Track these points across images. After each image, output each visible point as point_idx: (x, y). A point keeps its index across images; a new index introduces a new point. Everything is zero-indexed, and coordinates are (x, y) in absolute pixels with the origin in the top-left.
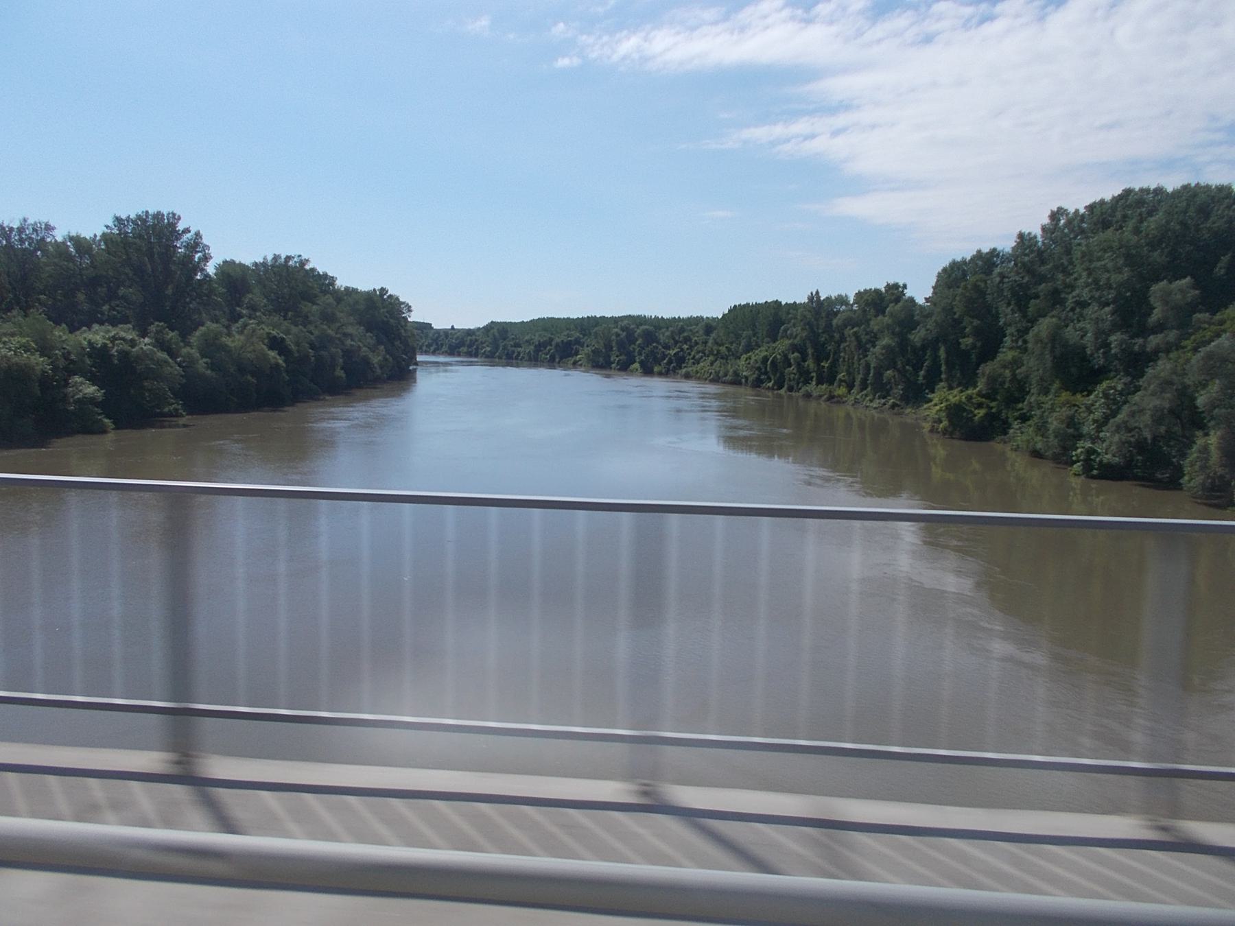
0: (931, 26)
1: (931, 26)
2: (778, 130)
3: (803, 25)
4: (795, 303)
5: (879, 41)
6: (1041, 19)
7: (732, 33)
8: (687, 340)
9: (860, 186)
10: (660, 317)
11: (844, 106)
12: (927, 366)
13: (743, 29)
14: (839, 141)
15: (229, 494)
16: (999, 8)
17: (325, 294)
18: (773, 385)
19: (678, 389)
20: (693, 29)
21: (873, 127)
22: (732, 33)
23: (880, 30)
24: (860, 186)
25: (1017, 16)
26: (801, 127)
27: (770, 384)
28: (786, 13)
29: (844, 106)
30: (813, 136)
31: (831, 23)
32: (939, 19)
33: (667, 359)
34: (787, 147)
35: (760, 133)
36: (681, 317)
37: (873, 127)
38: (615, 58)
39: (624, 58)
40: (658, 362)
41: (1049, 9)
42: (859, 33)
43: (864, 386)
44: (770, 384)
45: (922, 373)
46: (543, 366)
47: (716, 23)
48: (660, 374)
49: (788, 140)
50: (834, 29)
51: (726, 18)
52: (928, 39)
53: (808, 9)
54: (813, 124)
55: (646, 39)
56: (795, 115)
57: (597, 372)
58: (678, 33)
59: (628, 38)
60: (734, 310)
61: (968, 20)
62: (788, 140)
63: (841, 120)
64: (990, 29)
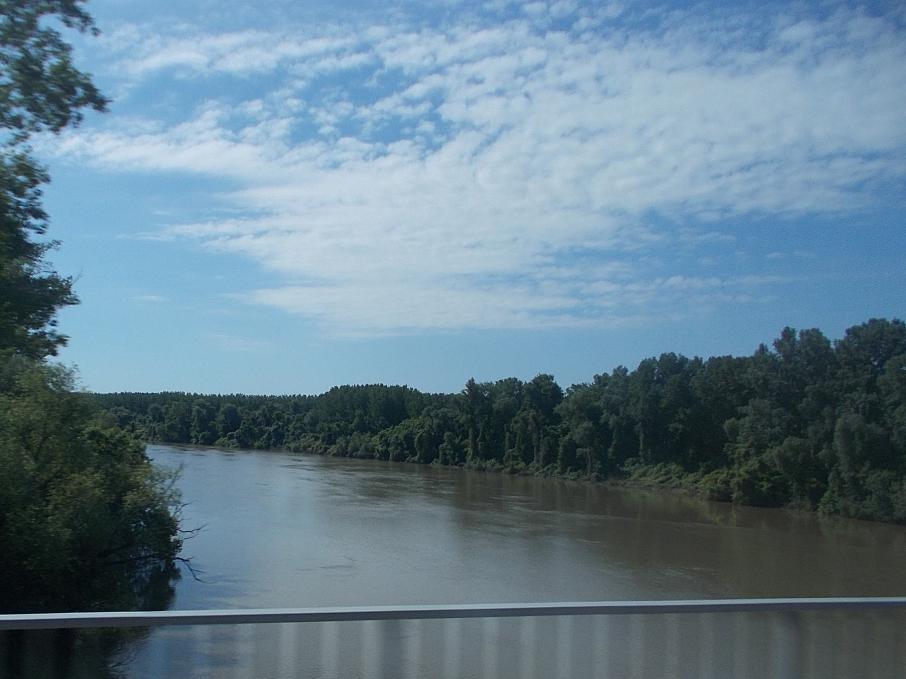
0: (340, 156)
1: (340, 156)
2: (208, 228)
3: (233, 143)
4: (405, 387)
5: (295, 163)
6: (422, 159)
7: (169, 144)
8: (279, 417)
9: (277, 280)
10: (192, 394)
11: (266, 213)
12: (614, 445)
13: (179, 142)
14: (261, 242)
15: (395, 618)
16: (391, 147)
17: (259, 408)
18: (419, 459)
19: (158, 451)
20: (133, 136)
21: (290, 232)
22: (169, 144)
23: (297, 154)
24: (277, 280)
25: (405, 154)
26: (227, 227)
27: (416, 458)
28: (218, 132)
29: (266, 213)
30: (238, 236)
31: (256, 144)
32: (345, 150)
33: (266, 435)
34: (216, 243)
35: (192, 230)
36: (222, 395)
37: (290, 232)
38: (58, 153)
39: (67, 154)
40: (256, 437)
41: (428, 152)
42: (279, 156)
43: (550, 458)
44: (416, 458)
45: (610, 450)
46: (302, 454)
47: (154, 133)
48: (260, 448)
49: (216, 238)
50: (259, 150)
51: (164, 130)
52: (335, 165)
53: (236, 131)
54: (238, 226)
55: (88, 140)
56: (223, 217)
57: (292, 457)
58: (120, 138)
59: (72, 138)
60: (334, 390)
61: (368, 154)
62: (216, 238)
63: (263, 224)
64: (382, 162)
